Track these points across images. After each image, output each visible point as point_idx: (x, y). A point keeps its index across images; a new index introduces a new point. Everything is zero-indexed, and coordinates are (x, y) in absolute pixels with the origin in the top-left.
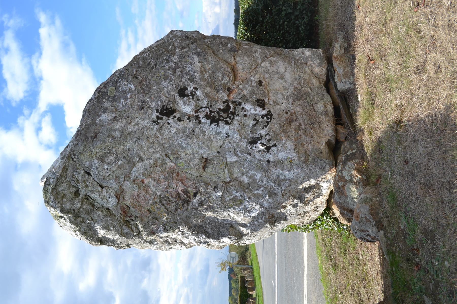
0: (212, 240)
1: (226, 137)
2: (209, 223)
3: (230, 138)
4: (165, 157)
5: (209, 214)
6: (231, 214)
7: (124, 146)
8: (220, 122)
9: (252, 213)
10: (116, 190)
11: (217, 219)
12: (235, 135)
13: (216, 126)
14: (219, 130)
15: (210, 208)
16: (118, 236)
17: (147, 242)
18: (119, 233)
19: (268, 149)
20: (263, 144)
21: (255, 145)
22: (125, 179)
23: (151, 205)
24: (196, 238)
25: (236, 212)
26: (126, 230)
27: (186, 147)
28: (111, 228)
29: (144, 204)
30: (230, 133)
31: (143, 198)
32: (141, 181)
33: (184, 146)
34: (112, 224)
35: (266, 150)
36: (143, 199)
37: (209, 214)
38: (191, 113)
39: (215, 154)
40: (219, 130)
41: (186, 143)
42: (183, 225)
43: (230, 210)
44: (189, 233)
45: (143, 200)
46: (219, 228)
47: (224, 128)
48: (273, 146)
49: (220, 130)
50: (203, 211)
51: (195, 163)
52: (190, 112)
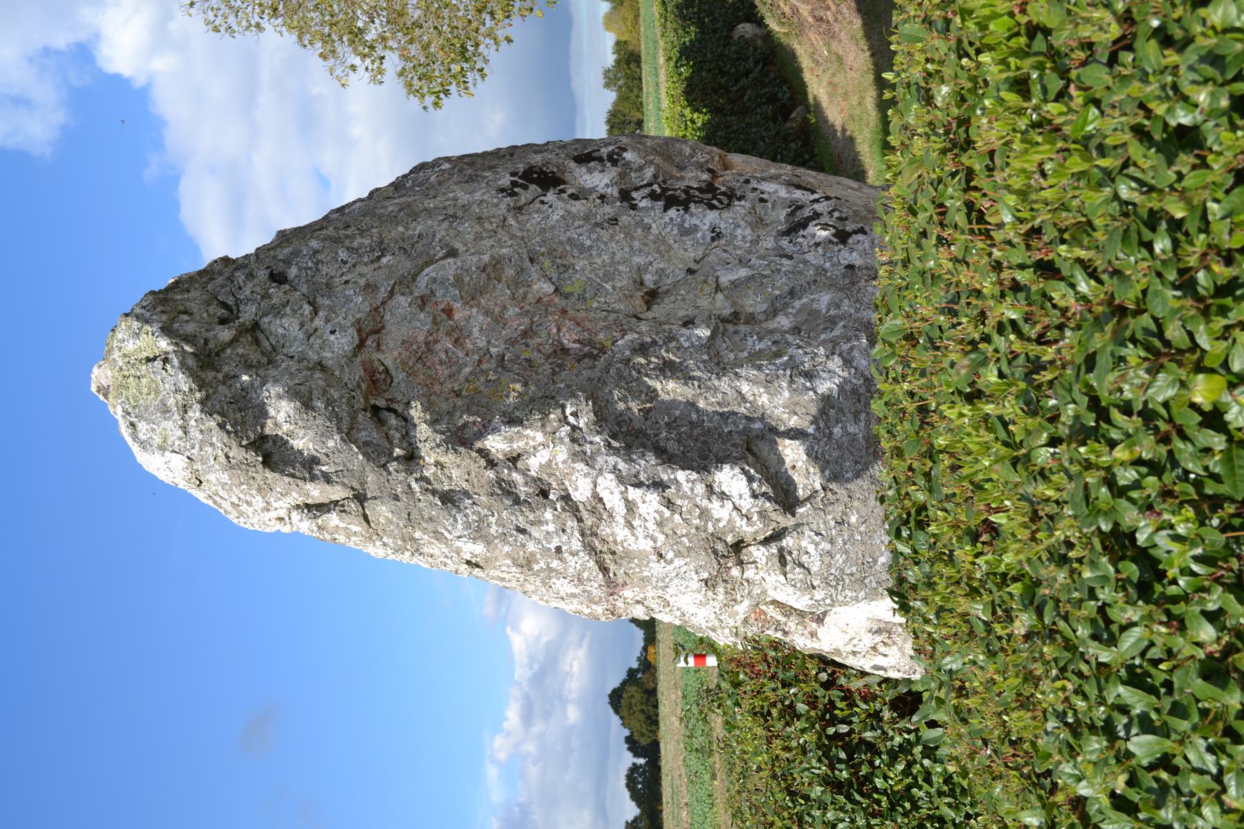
0: (681, 475)
1: (713, 239)
2: (667, 424)
3: (723, 242)
4: (527, 263)
5: (670, 389)
6: (745, 388)
7: (407, 229)
8: (692, 205)
9: (817, 382)
10: (358, 316)
11: (698, 410)
12: (739, 231)
13: (682, 212)
14: (690, 221)
15: (668, 369)
16: (337, 437)
17: (434, 492)
18: (340, 431)
19: (842, 237)
20: (825, 227)
21: (801, 233)
22: (397, 287)
23: (467, 380)
24: (622, 465)
25: (762, 377)
26: (369, 432)
27: (591, 247)
28: (319, 404)
29: (443, 372)
30: (723, 226)
31: (443, 356)
32: (443, 310)
33: (588, 243)
34: (325, 392)
35: (835, 240)
36: (440, 360)
37: (670, 389)
38: (609, 190)
39: (682, 275)
40: (690, 221)
41: (594, 236)
42: (577, 397)
43: (742, 372)
44: (597, 439)
45: (441, 363)
46: (704, 442)
47: (705, 216)
48: (855, 232)
49: (695, 221)
50: (647, 375)
51: (619, 285)
52: (607, 186)
